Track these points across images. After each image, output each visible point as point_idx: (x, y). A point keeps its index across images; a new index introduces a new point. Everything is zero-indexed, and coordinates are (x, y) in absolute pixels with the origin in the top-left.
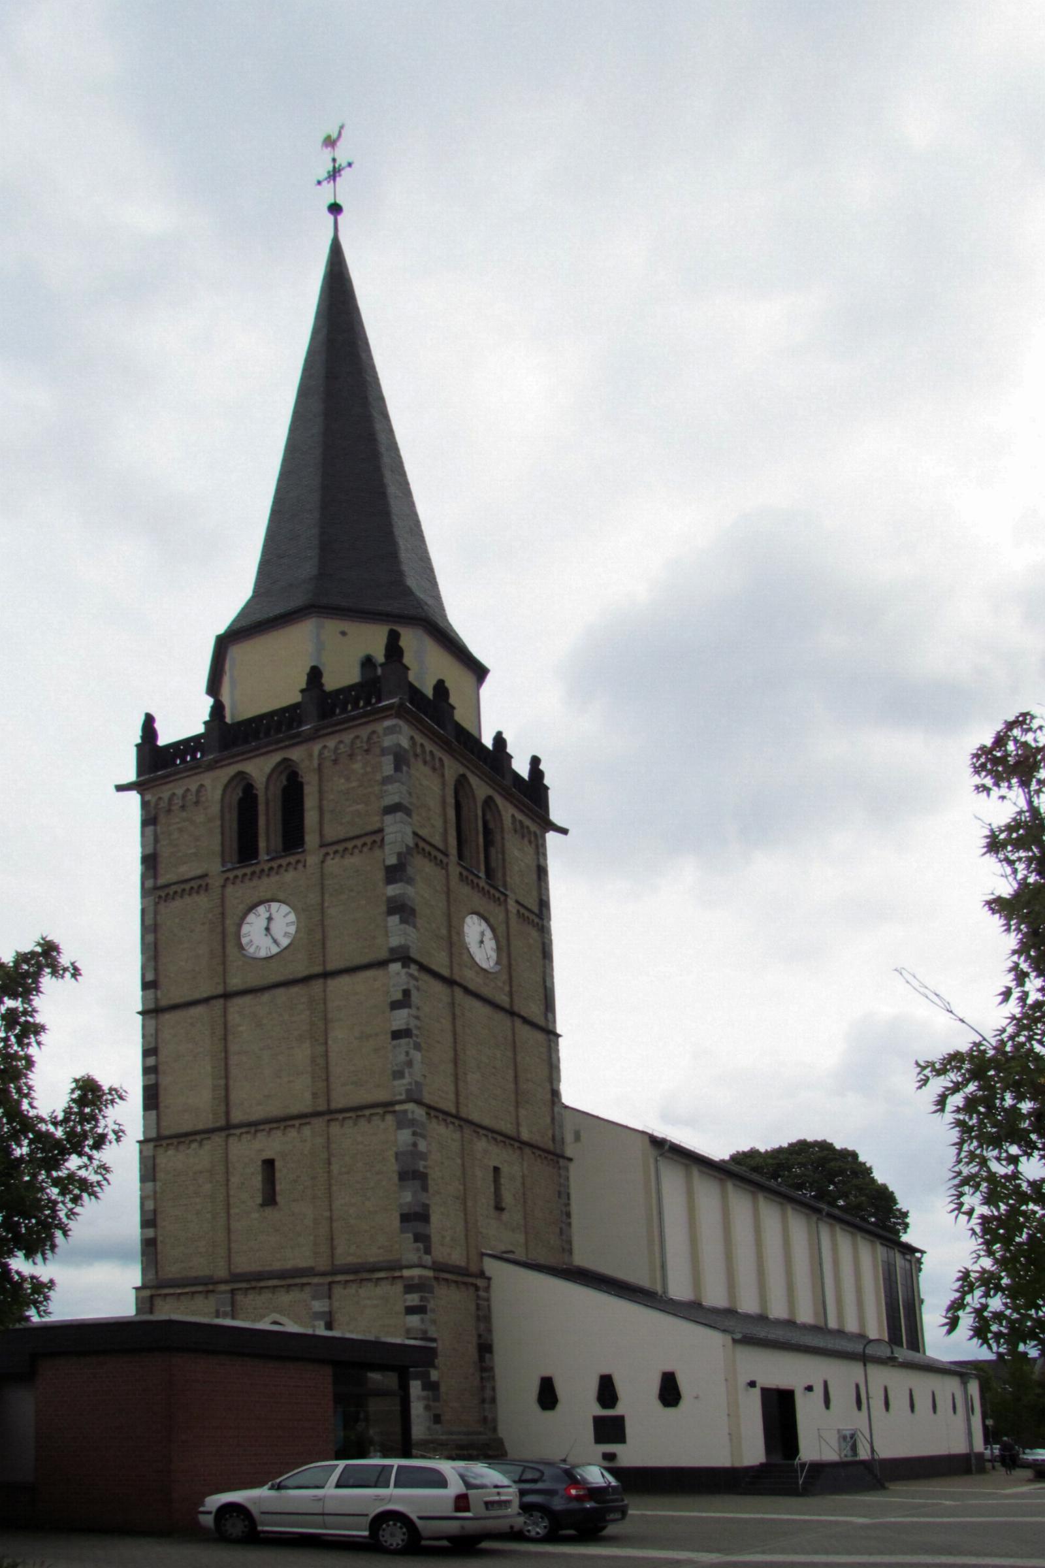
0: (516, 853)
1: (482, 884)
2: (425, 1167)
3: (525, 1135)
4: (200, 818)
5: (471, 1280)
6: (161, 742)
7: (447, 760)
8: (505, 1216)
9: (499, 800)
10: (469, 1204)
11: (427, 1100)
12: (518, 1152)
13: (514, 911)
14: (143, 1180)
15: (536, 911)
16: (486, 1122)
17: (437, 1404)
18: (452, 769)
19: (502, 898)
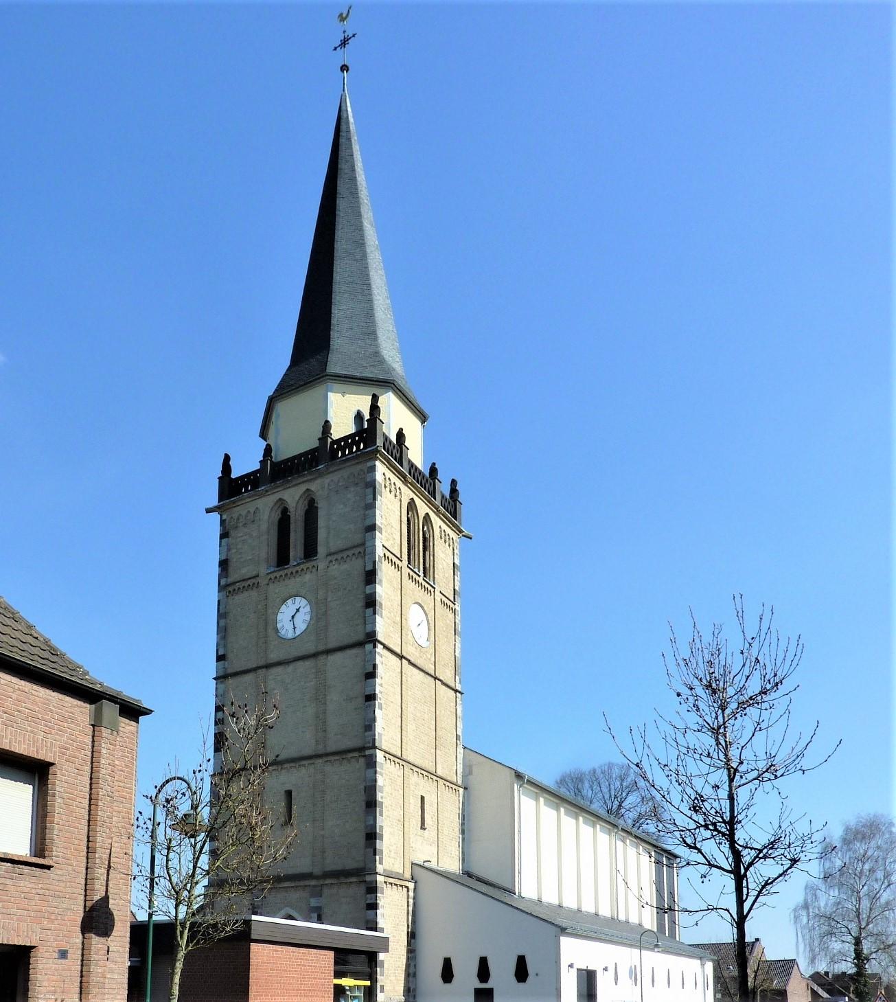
3: (439, 773)
6: (233, 476)
15: (452, 600)
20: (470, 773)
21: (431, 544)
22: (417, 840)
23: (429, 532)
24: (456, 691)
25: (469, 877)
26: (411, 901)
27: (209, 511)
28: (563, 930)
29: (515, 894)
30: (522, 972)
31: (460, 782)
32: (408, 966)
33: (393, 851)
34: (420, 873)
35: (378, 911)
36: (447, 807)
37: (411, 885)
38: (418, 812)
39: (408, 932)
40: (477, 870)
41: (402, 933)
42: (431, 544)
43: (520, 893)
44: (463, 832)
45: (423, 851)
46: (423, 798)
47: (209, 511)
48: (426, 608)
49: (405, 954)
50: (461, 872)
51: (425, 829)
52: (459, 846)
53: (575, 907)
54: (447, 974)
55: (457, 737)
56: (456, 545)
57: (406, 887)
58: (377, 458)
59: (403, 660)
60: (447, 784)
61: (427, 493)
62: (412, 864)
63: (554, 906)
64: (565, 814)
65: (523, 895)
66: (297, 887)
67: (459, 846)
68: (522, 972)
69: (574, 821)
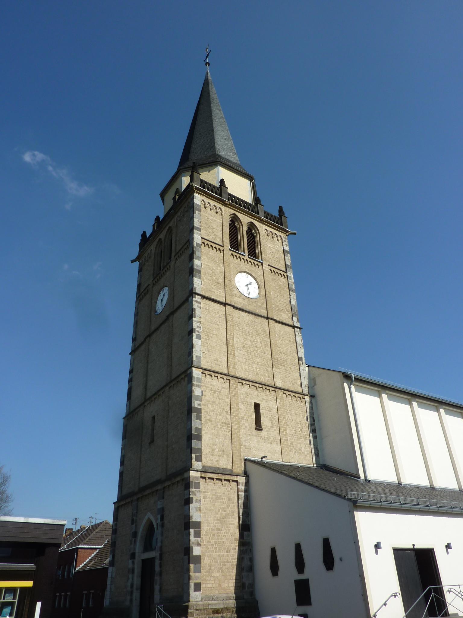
0: (269, 245)
1: (246, 258)
2: (200, 405)
3: (279, 384)
4: (224, 460)
5: (235, 478)
7: (223, 208)
8: (264, 433)
9: (257, 223)
10: (234, 426)
11: (203, 366)
12: (274, 393)
13: (268, 270)
14: (120, 466)
15: (284, 270)
16: (250, 377)
17: (197, 574)
18: (227, 212)
19: (259, 264)
20: (315, 384)
21: (258, 239)
22: (251, 439)
23: (256, 233)
24: (294, 327)
25: (323, 467)
26: (242, 494)
27: (132, 261)
28: (356, 505)
29: (359, 478)
30: (329, 561)
31: (306, 391)
32: (240, 559)
33: (217, 450)
34: (252, 468)
35: (191, 505)
36: (298, 413)
37: (242, 480)
38: (251, 416)
39: (239, 524)
40: (332, 462)
41: (232, 526)
42: (258, 239)
43: (365, 477)
44: (313, 431)
45: (265, 448)
46: (257, 406)
47: (132, 261)
48: (253, 275)
49: (237, 548)
50: (315, 466)
51: (261, 430)
52: (310, 443)
53: (427, 484)
54: (275, 569)
55: (300, 359)
56: (283, 240)
57: (234, 481)
58: (194, 192)
59: (227, 306)
60: (288, 393)
61: (211, 192)
62: (245, 460)
63: (427, 488)
64: (446, 414)
65: (369, 478)
66: (153, 492)
67: (310, 443)
68: (329, 561)
69: (408, 407)
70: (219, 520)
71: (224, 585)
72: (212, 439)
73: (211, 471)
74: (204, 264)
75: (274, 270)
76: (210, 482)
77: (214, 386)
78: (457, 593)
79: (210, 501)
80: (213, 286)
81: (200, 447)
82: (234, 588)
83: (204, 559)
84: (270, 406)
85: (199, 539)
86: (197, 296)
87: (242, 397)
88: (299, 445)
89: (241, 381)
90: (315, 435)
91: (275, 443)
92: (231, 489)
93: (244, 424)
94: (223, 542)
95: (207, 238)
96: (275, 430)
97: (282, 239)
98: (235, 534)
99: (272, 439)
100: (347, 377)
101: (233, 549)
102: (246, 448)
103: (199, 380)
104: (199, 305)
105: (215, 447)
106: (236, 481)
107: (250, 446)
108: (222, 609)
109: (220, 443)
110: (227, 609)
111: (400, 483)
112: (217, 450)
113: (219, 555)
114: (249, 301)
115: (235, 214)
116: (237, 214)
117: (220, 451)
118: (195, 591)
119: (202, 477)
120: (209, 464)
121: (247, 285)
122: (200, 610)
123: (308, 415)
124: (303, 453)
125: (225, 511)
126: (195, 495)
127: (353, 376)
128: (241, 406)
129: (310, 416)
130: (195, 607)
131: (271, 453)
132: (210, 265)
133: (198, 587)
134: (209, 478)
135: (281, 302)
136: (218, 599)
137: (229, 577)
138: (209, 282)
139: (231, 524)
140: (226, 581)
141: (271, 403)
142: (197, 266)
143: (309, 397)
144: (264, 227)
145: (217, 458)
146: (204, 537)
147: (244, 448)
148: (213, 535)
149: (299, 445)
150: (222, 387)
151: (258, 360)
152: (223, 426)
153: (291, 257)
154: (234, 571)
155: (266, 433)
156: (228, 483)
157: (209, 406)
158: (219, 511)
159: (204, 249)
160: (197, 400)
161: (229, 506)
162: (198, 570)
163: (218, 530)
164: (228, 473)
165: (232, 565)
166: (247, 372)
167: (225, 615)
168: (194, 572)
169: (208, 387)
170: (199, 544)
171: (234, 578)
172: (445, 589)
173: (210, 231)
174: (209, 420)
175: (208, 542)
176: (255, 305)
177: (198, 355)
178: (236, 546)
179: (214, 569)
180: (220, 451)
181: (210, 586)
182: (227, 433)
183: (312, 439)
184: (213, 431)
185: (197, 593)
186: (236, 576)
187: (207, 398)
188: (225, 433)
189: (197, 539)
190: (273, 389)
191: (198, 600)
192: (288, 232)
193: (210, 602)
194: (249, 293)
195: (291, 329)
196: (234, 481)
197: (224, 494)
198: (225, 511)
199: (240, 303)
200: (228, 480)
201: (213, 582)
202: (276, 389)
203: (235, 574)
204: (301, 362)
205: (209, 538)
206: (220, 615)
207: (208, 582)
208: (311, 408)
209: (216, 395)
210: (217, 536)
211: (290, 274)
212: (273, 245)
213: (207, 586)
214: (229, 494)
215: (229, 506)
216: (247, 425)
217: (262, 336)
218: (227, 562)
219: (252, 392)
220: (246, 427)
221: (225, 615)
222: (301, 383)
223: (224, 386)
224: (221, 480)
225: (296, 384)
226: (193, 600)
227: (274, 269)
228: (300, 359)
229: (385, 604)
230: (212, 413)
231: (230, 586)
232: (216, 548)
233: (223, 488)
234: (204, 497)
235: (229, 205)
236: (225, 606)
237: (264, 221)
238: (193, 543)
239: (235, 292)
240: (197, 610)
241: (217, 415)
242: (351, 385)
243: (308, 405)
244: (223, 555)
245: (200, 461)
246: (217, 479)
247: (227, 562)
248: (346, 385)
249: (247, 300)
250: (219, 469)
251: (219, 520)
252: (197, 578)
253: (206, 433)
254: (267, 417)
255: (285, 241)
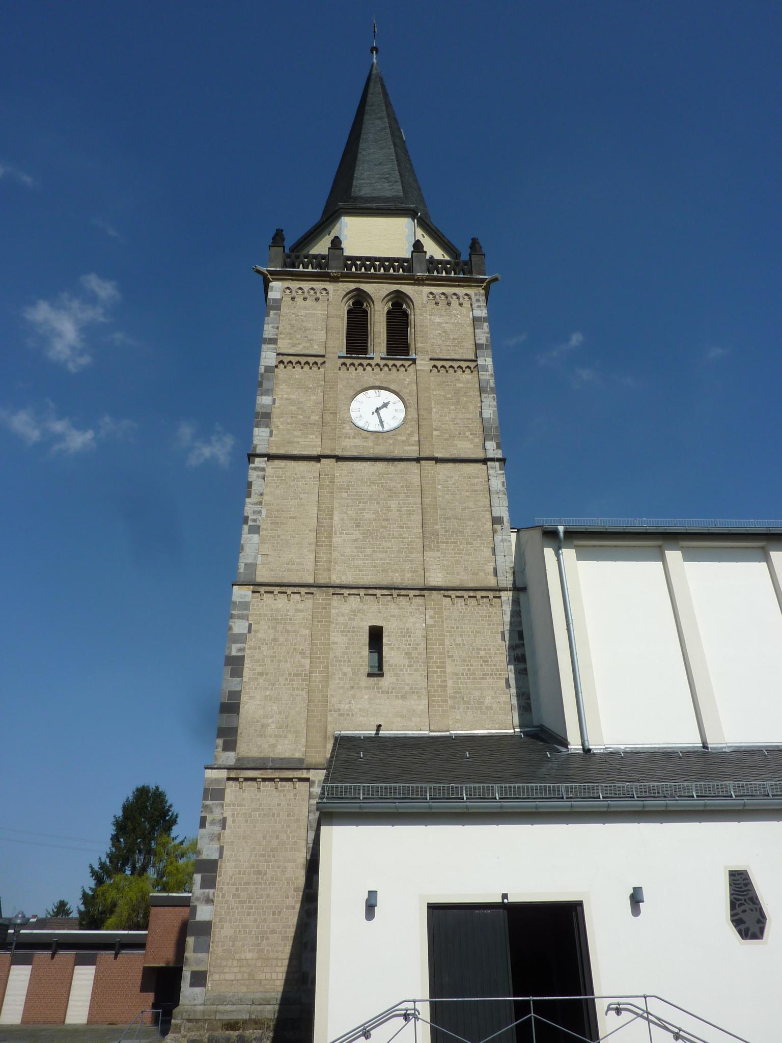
4: (286, 742)
5: (304, 774)
9: (407, 289)
17: (200, 955)
18: (337, 294)
29: (565, 744)
48: (392, 387)
49: (298, 906)
52: (508, 686)
57: (301, 780)
60: (453, 594)
69: (764, 565)
70: (264, 856)
71: (262, 976)
72: (264, 707)
73: (249, 766)
74: (282, 399)
75: (441, 364)
76: (250, 786)
77: (278, 610)
78: (640, 1012)
79: (247, 821)
80: (296, 433)
81: (235, 725)
82: (283, 982)
83: (222, 927)
84: (408, 626)
85: (211, 891)
86: (257, 460)
87: (341, 620)
88: (477, 693)
89: (338, 591)
90: (522, 666)
91: (415, 696)
92: (295, 795)
93: (341, 670)
94: (268, 896)
95: (291, 352)
96: (416, 670)
97: (470, 298)
98: (297, 879)
99: (407, 688)
100: (550, 535)
101: (288, 908)
102: (340, 715)
103: (245, 605)
104: (261, 473)
105: (270, 721)
106: (307, 780)
107: (350, 710)
108: (245, 1022)
109: (280, 713)
110: (256, 1023)
111: (587, 751)
112: (273, 726)
113: (255, 920)
114: (377, 438)
115: (358, 289)
116: (363, 287)
117: (281, 727)
118: (193, 985)
119: (229, 779)
120: (254, 753)
121: (377, 410)
122: (197, 1021)
123: (508, 627)
124: (489, 708)
125: (277, 837)
126: (212, 812)
127: (561, 529)
128: (338, 638)
129: (511, 631)
130: (185, 1016)
131: (402, 716)
132: (292, 397)
133: (199, 979)
134: (246, 779)
135: (457, 421)
136: (241, 1001)
137: (274, 962)
138: (289, 427)
139: (289, 861)
140: (267, 969)
141: (412, 620)
142: (263, 406)
143: (510, 594)
144: (426, 290)
145: (272, 741)
146: (225, 887)
147: (336, 714)
148: (246, 883)
149: (477, 693)
150: (297, 610)
151: (389, 544)
152: (292, 680)
153: (490, 327)
154: (288, 949)
155: (394, 680)
156: (288, 785)
157: (264, 648)
158: (264, 837)
159: (281, 372)
160: (235, 642)
161: (289, 826)
162: (203, 948)
163: (259, 872)
164: (293, 766)
165: (285, 938)
166: (360, 570)
167: (248, 1033)
168: (194, 951)
169: (265, 615)
170: (209, 901)
171: (286, 962)
172: (601, 1006)
173: (298, 336)
174: (261, 674)
175: (234, 895)
176: (391, 441)
177: (250, 561)
178: (296, 902)
179: (243, 946)
180: (281, 727)
181: (230, 977)
182: (299, 692)
183: (512, 676)
184: (268, 693)
185: (198, 990)
186: (291, 959)
187: (259, 635)
188: (296, 692)
189: (207, 891)
190: (417, 593)
191: (196, 1002)
192: (483, 281)
193: (221, 1008)
194: (381, 422)
195: (480, 466)
196: (301, 780)
197: (279, 805)
198: (277, 837)
199: (356, 447)
200: (290, 780)
201: (237, 970)
202: (423, 593)
203: (287, 956)
204: (498, 527)
205: (237, 889)
206: (237, 1033)
207: (227, 970)
208: (516, 614)
209: (280, 627)
210: (255, 884)
211: (486, 361)
212: (448, 320)
213: (222, 977)
214: (289, 805)
215: (289, 826)
216: (347, 670)
217: (402, 496)
218: (273, 932)
219: (365, 607)
220: (345, 674)
221: (248, 1033)
222: (495, 570)
223: (301, 606)
224: (272, 780)
225: (482, 574)
226: (187, 1002)
227: (450, 363)
228: (497, 521)
229: (366, 1035)
230: (267, 661)
231: (274, 976)
232: (251, 908)
233: (277, 794)
234: (233, 815)
235: (341, 277)
236: (253, 1017)
237: (423, 280)
238: (198, 899)
239: (347, 429)
240: (189, 1020)
241: (280, 661)
242: (560, 548)
243: (508, 608)
244: (265, 920)
245: (233, 748)
246: (264, 780)
247: (273, 932)
248: (549, 553)
249: (372, 437)
250: (273, 760)
251: (264, 856)
252: (199, 962)
253: (252, 698)
254: (398, 649)
255: (478, 301)
